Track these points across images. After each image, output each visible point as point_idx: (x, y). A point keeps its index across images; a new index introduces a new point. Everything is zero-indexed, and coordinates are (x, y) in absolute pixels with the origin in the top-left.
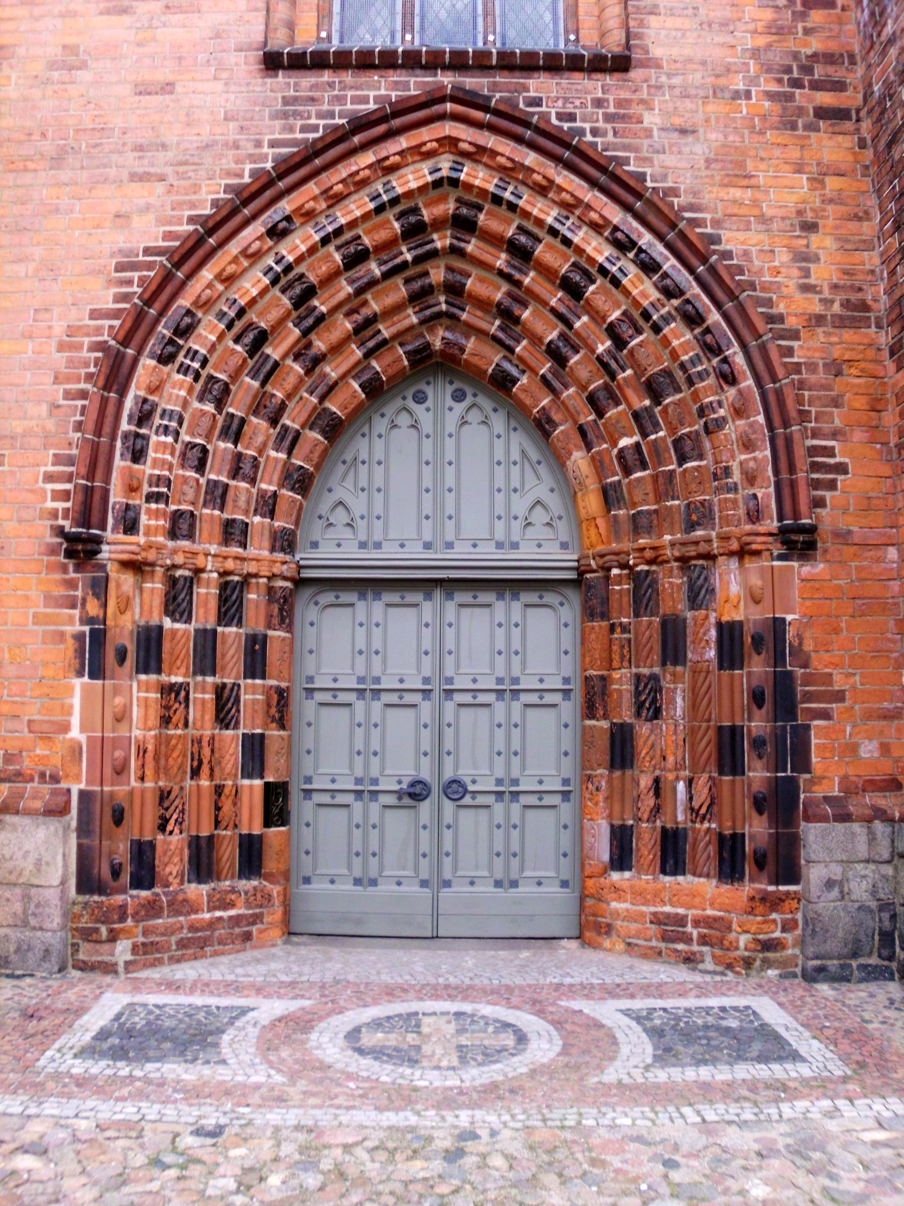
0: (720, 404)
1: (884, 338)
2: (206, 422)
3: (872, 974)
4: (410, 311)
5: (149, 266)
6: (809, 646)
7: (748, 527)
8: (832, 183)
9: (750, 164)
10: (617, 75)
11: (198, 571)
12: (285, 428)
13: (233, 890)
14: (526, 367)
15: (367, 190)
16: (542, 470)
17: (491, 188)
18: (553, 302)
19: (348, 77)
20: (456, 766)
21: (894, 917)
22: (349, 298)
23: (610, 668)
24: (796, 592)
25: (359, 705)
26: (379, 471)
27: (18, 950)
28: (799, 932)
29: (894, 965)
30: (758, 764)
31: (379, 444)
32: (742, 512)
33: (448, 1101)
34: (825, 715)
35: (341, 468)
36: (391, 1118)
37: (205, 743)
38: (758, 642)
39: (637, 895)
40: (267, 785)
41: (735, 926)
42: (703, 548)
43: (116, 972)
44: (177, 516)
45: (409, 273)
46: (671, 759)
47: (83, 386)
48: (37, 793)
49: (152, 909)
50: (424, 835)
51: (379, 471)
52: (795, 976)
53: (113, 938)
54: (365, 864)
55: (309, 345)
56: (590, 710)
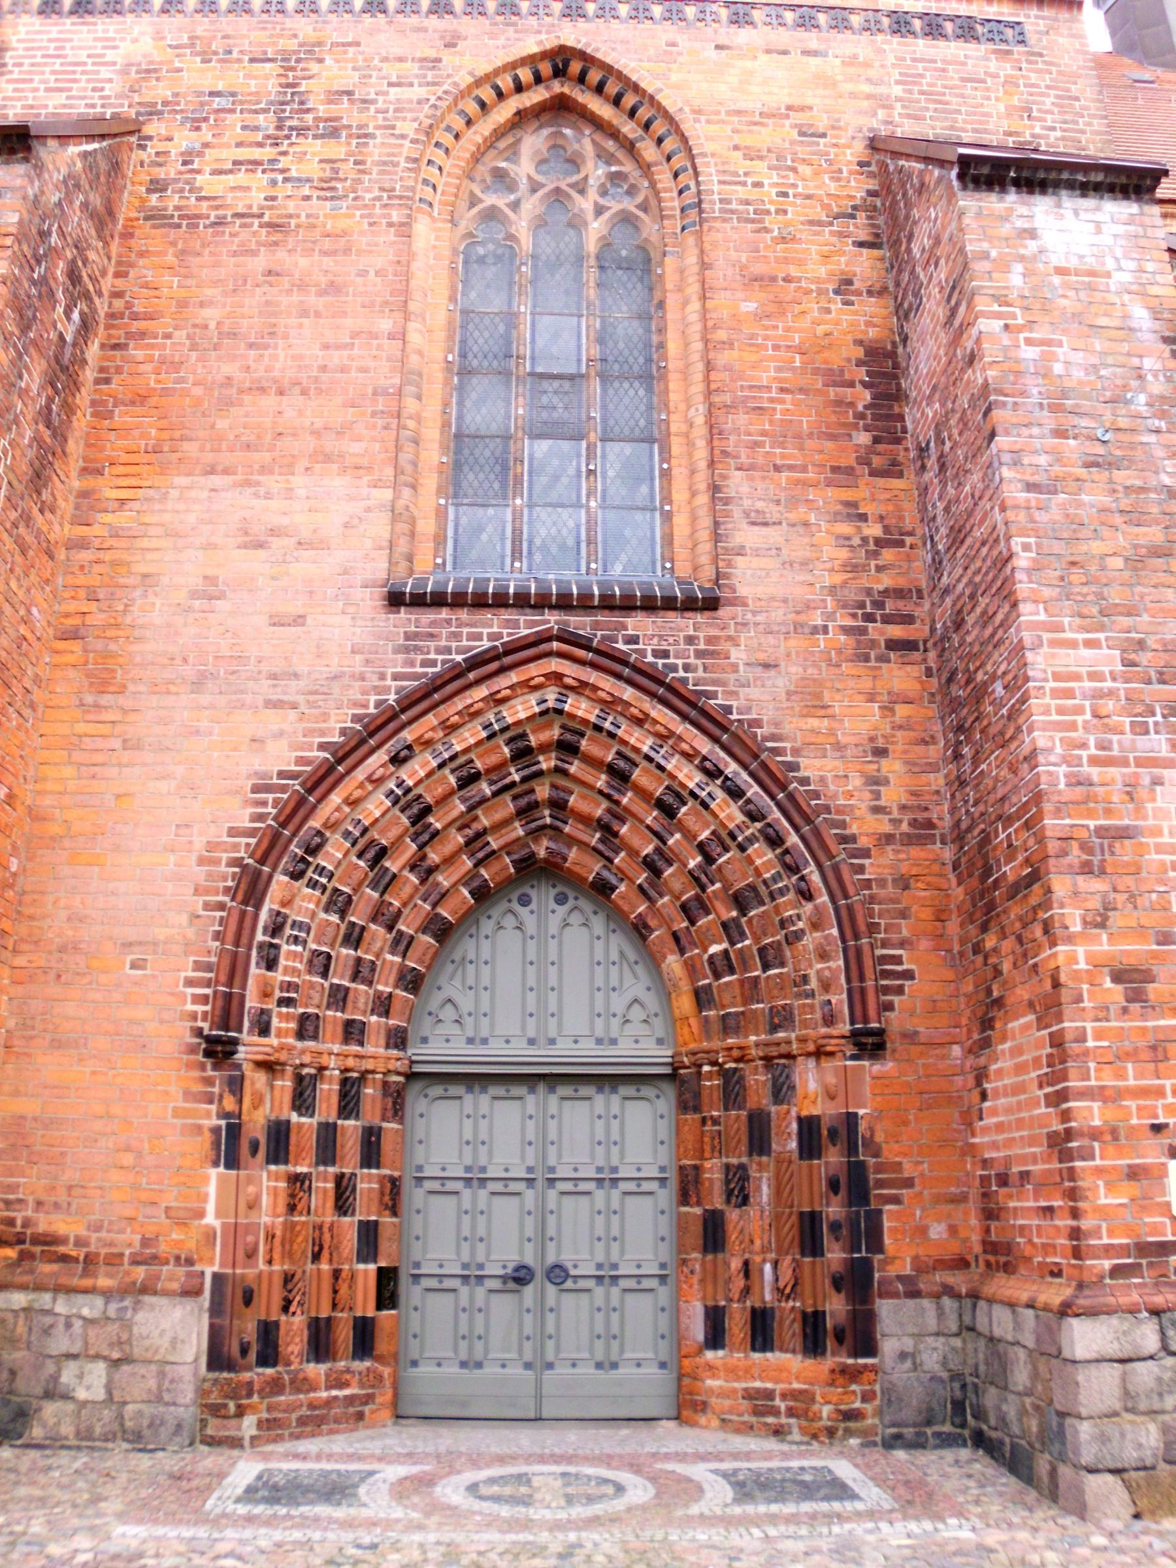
0: (799, 917)
1: (948, 854)
2: (330, 931)
3: (947, 1441)
4: (517, 824)
5: (283, 789)
6: (879, 1137)
7: (824, 1030)
8: (902, 710)
9: (826, 695)
10: (707, 614)
11: (322, 1068)
12: (400, 933)
13: (348, 1371)
14: (623, 876)
15: (480, 720)
16: (639, 969)
17: (593, 719)
18: (649, 821)
19: (464, 614)
20: (559, 1252)
21: (964, 1387)
22: (462, 814)
23: (702, 1158)
24: (868, 1091)
25: (467, 1193)
26: (486, 970)
27: (150, 1425)
28: (877, 1402)
29: (966, 1433)
30: (836, 1246)
31: (486, 945)
32: (818, 1015)
33: (556, 1526)
34: (896, 1200)
35: (450, 968)
36: (512, 1537)
37: (326, 1229)
38: (833, 1134)
39: (729, 1371)
40: (380, 1269)
41: (818, 1398)
42: (784, 1049)
43: (242, 1447)
44: (304, 1019)
45: (515, 791)
46: (758, 1243)
47: (221, 898)
48: (172, 1275)
49: (276, 1386)
50: (528, 1319)
51: (486, 970)
52: (875, 1444)
53: (240, 1413)
54: (471, 1348)
55: (424, 857)
56: (684, 1197)
